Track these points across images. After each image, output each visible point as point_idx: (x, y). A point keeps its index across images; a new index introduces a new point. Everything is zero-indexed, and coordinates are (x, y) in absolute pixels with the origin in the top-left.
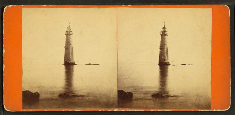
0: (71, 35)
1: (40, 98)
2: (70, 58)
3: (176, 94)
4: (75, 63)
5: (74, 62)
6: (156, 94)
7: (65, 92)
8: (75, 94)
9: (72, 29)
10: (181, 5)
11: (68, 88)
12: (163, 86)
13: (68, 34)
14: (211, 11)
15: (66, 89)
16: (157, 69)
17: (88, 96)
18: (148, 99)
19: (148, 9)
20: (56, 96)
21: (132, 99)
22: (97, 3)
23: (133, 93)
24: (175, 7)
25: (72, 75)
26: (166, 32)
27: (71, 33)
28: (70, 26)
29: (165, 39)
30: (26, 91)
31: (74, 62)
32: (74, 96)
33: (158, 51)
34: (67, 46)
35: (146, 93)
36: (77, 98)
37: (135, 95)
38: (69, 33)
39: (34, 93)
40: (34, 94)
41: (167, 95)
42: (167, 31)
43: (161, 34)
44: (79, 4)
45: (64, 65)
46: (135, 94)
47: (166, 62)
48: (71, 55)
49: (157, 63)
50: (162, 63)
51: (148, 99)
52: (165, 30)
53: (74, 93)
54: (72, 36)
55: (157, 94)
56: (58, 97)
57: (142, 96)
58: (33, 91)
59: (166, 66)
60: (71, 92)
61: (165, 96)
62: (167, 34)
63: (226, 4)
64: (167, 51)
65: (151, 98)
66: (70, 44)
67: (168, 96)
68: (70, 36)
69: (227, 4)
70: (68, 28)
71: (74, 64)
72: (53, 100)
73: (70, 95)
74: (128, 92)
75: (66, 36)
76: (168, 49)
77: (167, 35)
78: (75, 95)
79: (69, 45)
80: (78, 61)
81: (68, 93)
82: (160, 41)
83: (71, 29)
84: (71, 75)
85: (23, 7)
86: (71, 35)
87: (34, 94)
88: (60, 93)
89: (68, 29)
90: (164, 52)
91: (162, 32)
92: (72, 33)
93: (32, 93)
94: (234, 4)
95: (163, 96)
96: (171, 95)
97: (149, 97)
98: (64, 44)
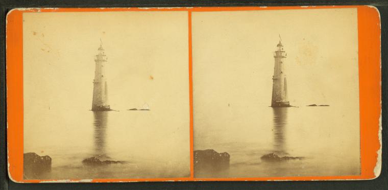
0: (104, 61)
1: (231, 162)
2: (103, 99)
3: (123, 160)
6: (268, 155)
7: (273, 151)
9: (286, 48)
10: (336, 6)
11: (99, 150)
13: (279, 56)
15: (97, 150)
16: (270, 113)
18: (256, 164)
19: (97, 13)
20: (79, 162)
22: (162, 3)
23: (229, 154)
25: (105, 128)
26: (103, 55)
27: (283, 54)
28: (281, 43)
29: (282, 64)
30: (29, 153)
32: (108, 162)
34: (277, 76)
35: (252, 154)
36: (113, 165)
37: (233, 159)
38: (279, 54)
40: (221, 155)
41: (108, 160)
42: (284, 50)
43: (275, 55)
45: (92, 110)
46: (233, 155)
47: (284, 101)
48: (103, 92)
49: (270, 103)
50: (276, 103)
51: (256, 164)
52: (281, 48)
54: (284, 59)
55: (270, 154)
57: (246, 158)
58: (219, 150)
59: (284, 108)
60: (104, 156)
61: (284, 158)
63: (375, 4)
64: (106, 86)
65: (260, 161)
66: (102, 76)
67: (288, 158)
68: (103, 63)
69: (377, 5)
70: (278, 46)
71: (109, 110)
72: (73, 168)
73: (102, 161)
74: (223, 152)
75: (274, 59)
76: (108, 84)
78: (111, 160)
80: (294, 101)
81: (278, 152)
82: (95, 70)
84: (103, 128)
86: (104, 61)
88: (86, 156)
89: (100, 51)
90: (280, 86)
92: (106, 57)
93: (40, 157)
95: (279, 158)
96: (114, 160)
97: (257, 159)
98: (92, 77)
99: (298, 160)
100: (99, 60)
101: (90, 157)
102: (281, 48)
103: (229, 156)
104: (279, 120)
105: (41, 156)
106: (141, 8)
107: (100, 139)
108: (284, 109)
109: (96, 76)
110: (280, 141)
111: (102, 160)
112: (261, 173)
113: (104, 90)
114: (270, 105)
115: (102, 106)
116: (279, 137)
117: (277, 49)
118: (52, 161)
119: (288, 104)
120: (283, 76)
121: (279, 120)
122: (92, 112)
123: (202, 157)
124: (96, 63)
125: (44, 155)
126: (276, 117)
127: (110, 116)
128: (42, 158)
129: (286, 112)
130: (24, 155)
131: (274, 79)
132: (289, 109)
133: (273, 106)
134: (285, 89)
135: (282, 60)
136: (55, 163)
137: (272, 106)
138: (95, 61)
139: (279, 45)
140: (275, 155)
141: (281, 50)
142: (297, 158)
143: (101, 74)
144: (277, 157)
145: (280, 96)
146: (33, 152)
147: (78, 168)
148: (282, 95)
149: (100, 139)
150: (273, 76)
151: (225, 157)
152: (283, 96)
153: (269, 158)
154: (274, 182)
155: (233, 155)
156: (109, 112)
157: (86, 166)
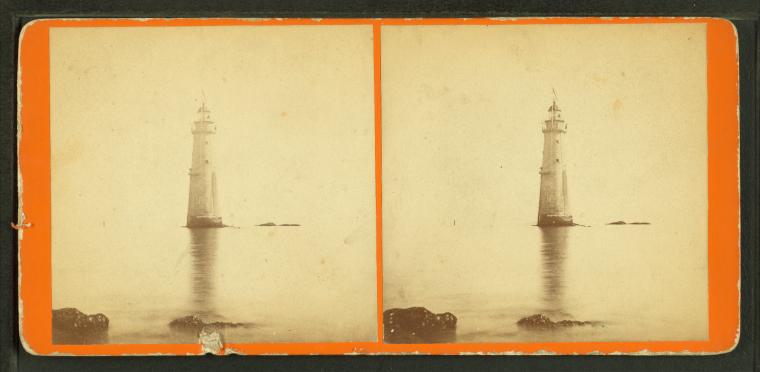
1: (458, 332)
4: (224, 223)
5: (220, 218)
8: (225, 319)
11: (200, 301)
12: (554, 291)
14: (55, 29)
17: (262, 326)
20: (162, 325)
21: (454, 334)
23: (457, 316)
24: (309, 24)
27: (561, 126)
31: (220, 218)
33: (534, 183)
36: (576, 329)
39: (91, 316)
40: (439, 318)
41: (567, 320)
42: (562, 119)
44: (261, 13)
45: (187, 227)
47: (561, 214)
48: (209, 194)
49: (183, 219)
53: (219, 316)
54: (212, 135)
55: (187, 318)
56: (168, 329)
60: (559, 311)
61: (562, 322)
62: (214, 131)
65: (515, 328)
67: (570, 323)
70: (550, 110)
76: (568, 174)
77: (565, 132)
78: (225, 321)
79: (554, 163)
83: (562, 114)
85: (386, 24)
87: (439, 318)
90: (555, 185)
91: (547, 122)
94: (757, 19)
99: (588, 328)
100: (552, 128)
101: (183, 316)
102: (557, 115)
103: (455, 319)
104: (553, 253)
105: (89, 314)
106: (496, 19)
107: (203, 284)
108: (562, 230)
109: (546, 160)
110: (554, 291)
111: (554, 320)
112: (518, 344)
113: (210, 183)
114: (536, 221)
115: (208, 218)
116: (553, 285)
117: (548, 116)
118: (458, 324)
119: (218, 221)
120: (559, 169)
121: (553, 253)
122: (538, 229)
123: (403, 321)
124: (195, 138)
125: (95, 313)
126: (546, 247)
127: (222, 239)
128: (90, 319)
129: (565, 238)
130: (55, 313)
131: (191, 175)
132: (220, 231)
133: (540, 224)
134: (565, 192)
135: (558, 137)
136: (463, 326)
137: (540, 224)
138: (544, 131)
139: (553, 109)
140: (544, 318)
141: (557, 118)
142: (587, 323)
143: (203, 157)
144: (548, 321)
145: (555, 204)
146: (72, 307)
147: (162, 336)
148: (558, 204)
149: (203, 284)
150: (191, 169)
151: (448, 323)
152: (560, 205)
153: (532, 322)
154: (186, 357)
155: (463, 317)
156: (571, 229)
157: (177, 334)
